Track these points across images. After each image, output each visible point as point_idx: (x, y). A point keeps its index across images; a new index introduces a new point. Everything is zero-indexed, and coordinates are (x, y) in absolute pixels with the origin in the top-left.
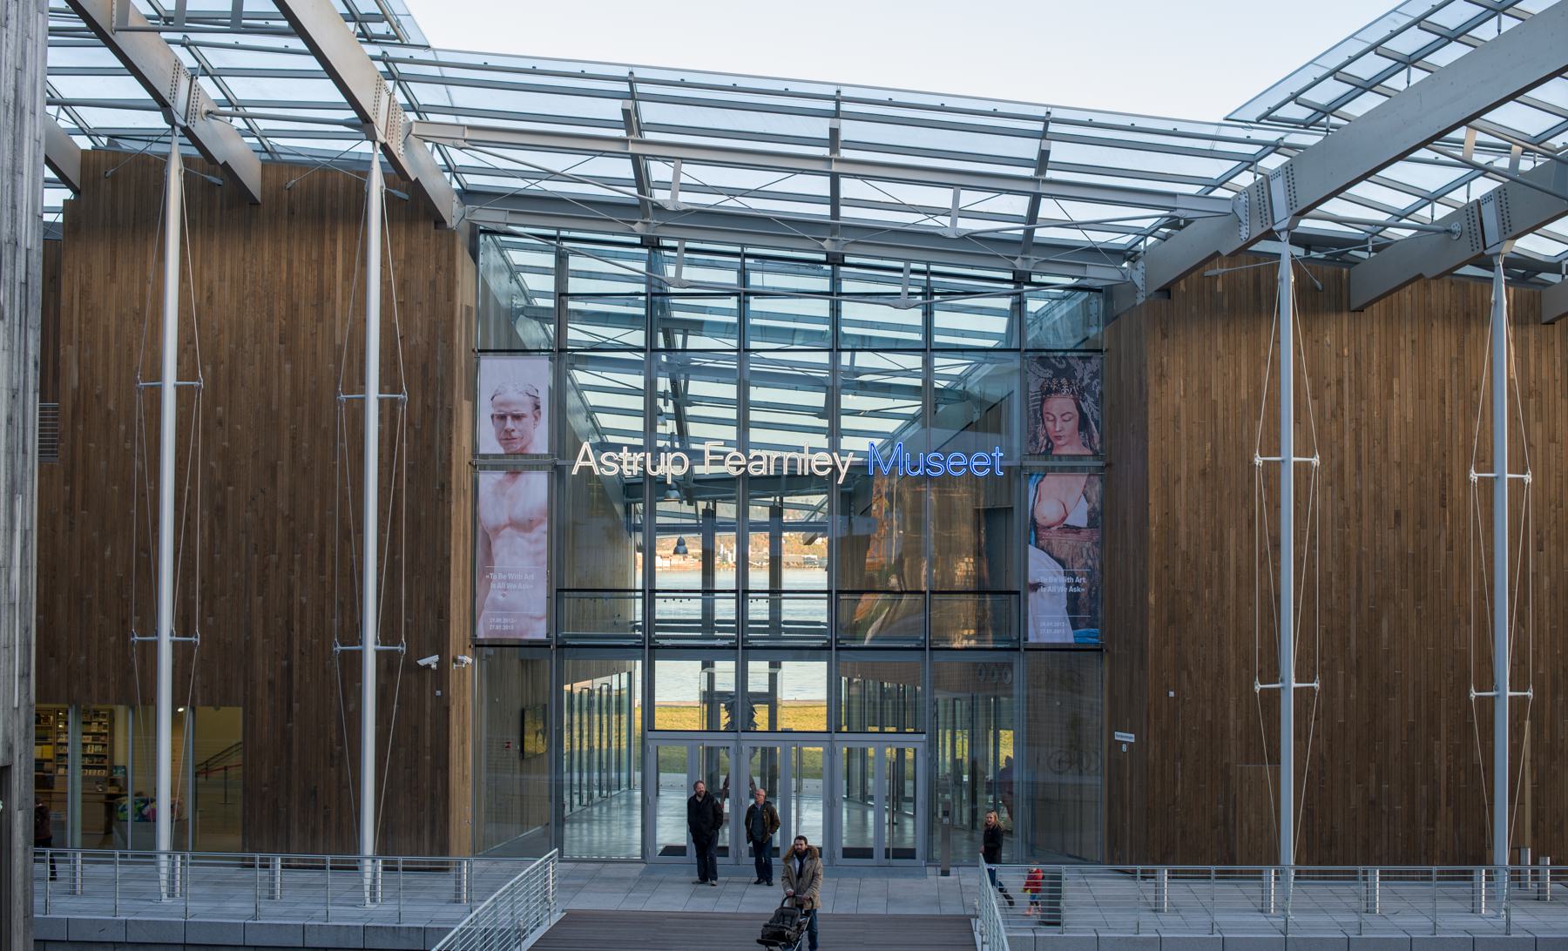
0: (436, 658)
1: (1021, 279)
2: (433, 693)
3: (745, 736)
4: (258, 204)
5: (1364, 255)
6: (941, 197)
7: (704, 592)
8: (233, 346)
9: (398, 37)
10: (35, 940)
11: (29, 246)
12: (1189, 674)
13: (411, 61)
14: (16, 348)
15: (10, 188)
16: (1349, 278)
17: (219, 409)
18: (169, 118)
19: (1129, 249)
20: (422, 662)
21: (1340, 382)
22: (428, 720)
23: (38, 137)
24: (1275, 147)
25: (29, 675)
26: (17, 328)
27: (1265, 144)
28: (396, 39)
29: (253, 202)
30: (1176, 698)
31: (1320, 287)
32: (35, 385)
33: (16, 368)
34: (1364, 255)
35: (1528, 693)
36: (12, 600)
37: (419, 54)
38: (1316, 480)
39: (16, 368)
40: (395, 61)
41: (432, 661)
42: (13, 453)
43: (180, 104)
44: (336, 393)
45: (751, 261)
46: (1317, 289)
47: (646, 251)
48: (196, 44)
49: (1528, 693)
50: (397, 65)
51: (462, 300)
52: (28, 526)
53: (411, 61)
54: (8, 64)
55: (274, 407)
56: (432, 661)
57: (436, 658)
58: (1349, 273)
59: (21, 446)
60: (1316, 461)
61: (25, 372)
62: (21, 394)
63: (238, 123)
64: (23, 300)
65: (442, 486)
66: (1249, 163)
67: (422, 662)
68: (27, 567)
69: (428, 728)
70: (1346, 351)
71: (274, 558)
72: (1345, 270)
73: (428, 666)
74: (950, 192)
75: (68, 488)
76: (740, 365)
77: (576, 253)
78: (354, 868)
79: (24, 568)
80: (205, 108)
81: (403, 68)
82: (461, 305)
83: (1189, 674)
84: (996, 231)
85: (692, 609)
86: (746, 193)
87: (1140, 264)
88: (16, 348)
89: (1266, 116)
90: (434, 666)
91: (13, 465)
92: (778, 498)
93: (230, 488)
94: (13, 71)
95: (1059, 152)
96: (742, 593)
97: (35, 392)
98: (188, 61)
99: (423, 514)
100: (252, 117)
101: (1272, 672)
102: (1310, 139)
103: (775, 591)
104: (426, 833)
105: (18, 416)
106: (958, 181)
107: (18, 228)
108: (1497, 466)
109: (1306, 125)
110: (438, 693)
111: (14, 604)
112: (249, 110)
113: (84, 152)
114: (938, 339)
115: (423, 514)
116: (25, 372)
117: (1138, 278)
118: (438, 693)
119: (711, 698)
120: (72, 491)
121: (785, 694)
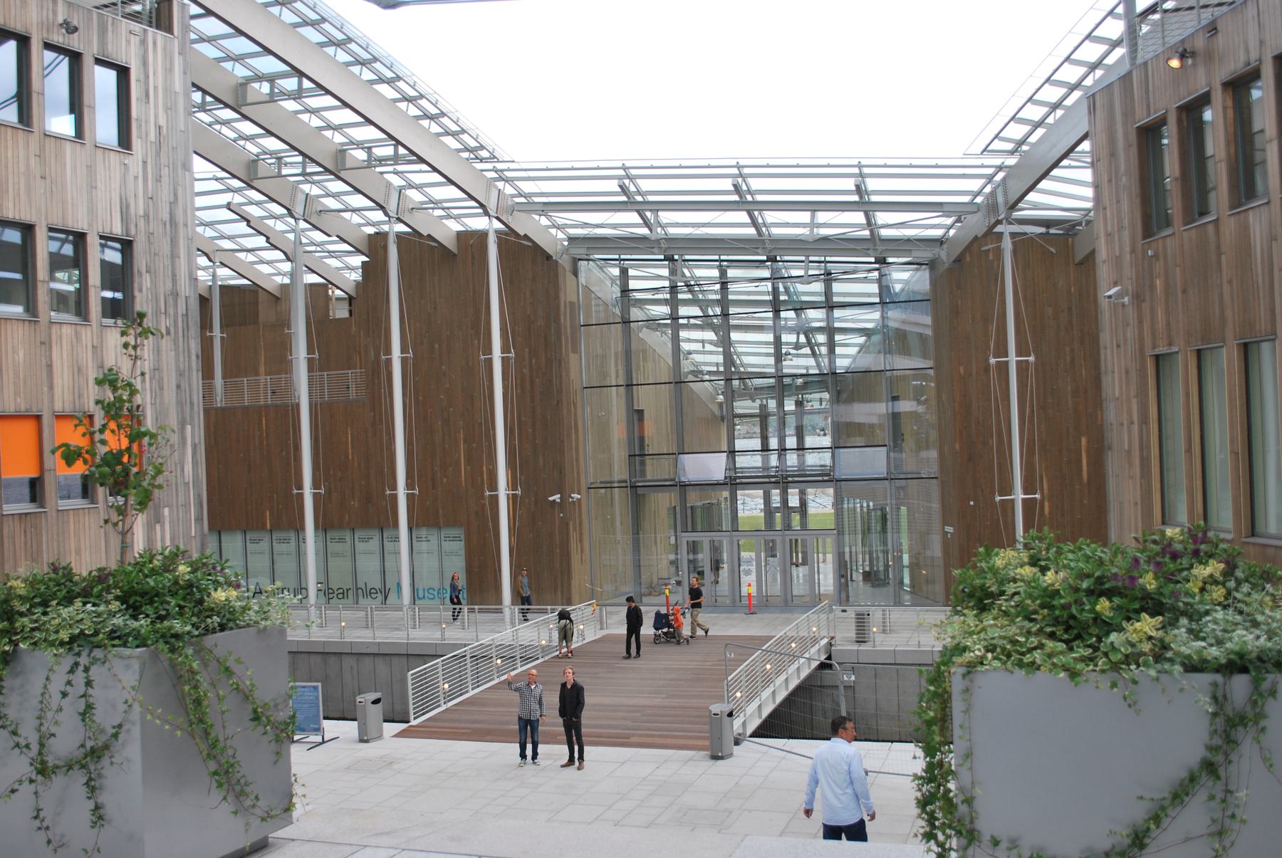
0: (559, 496)
1: (882, 261)
2: (559, 515)
3: (787, 532)
4: (456, 255)
5: (1081, 228)
6: (805, 217)
7: (798, 449)
8: (448, 333)
9: (495, 157)
10: (289, 652)
11: (187, 295)
12: (982, 491)
13: (509, 170)
14: (181, 349)
15: (170, 267)
16: (1073, 244)
17: (443, 367)
18: (386, 214)
19: (943, 237)
20: (551, 499)
21: (1070, 309)
22: (557, 530)
23: (190, 237)
24: (1000, 168)
25: (202, 519)
26: (181, 339)
27: (996, 167)
28: (493, 157)
29: (454, 255)
30: (975, 505)
31: (1054, 252)
32: (197, 367)
33: (181, 359)
34: (1081, 228)
35: (1036, 496)
36: (186, 480)
37: (512, 166)
38: (1032, 370)
39: (181, 359)
40: (502, 171)
41: (557, 497)
42: (182, 404)
43: (392, 208)
44: (479, 356)
45: (725, 263)
46: (1052, 253)
47: (667, 263)
48: (402, 172)
49: (1036, 496)
50: (505, 173)
51: (566, 298)
52: (197, 441)
53: (509, 170)
54: (164, 200)
55: (471, 364)
56: (557, 497)
57: (559, 496)
58: (1073, 242)
59: (188, 400)
60: (1032, 359)
61: (189, 361)
62: (187, 373)
63: (440, 213)
64: (185, 324)
65: (558, 402)
66: (990, 178)
67: (551, 499)
68: (197, 464)
69: (557, 534)
70: (1073, 289)
71: (474, 445)
72: (1070, 240)
73: (554, 500)
74: (809, 214)
75: (372, 414)
76: (774, 323)
77: (632, 267)
78: (500, 611)
79: (195, 463)
80: (411, 206)
81: (508, 174)
82: (565, 302)
83: (982, 491)
84: (844, 234)
85: (756, 461)
86: (704, 225)
87: (945, 246)
88: (181, 349)
89: (985, 150)
90: (558, 500)
91: (182, 411)
92: (800, 396)
93: (451, 409)
94: (168, 204)
95: (872, 184)
96: (782, 450)
97: (198, 371)
98: (396, 181)
99: (549, 417)
100: (448, 208)
101: (1007, 488)
102: (1011, 161)
103: (801, 448)
104: (559, 589)
105: (184, 385)
106: (814, 207)
107: (178, 287)
108: (1009, 354)
109: (1012, 152)
110: (562, 515)
111: (189, 483)
112: (446, 205)
113: (370, 235)
114: (835, 299)
115: (549, 417)
116: (189, 361)
117: (943, 255)
118: (562, 515)
119: (769, 511)
120: (374, 415)
121: (812, 509)
